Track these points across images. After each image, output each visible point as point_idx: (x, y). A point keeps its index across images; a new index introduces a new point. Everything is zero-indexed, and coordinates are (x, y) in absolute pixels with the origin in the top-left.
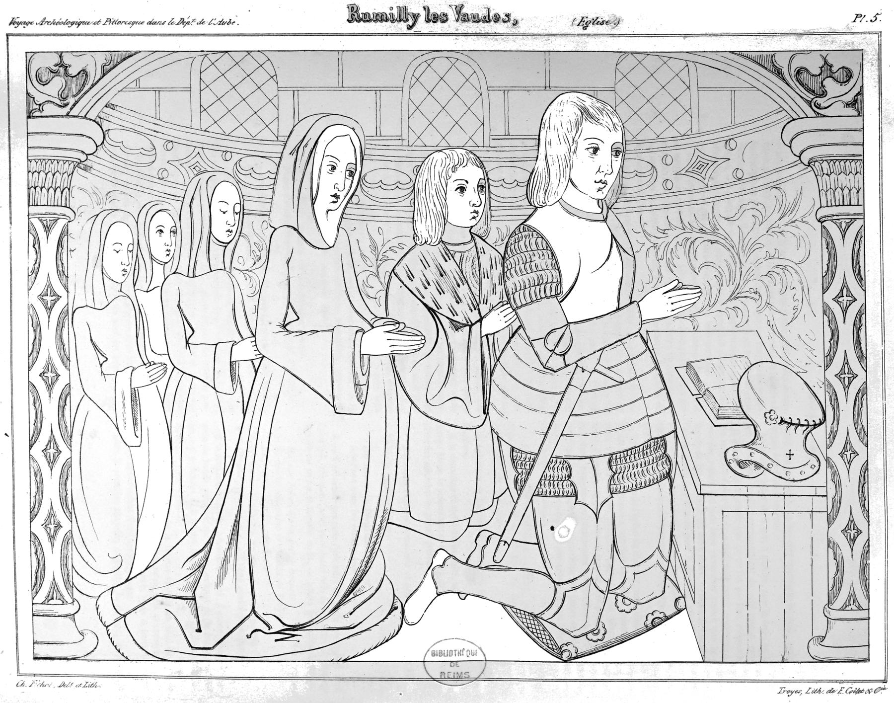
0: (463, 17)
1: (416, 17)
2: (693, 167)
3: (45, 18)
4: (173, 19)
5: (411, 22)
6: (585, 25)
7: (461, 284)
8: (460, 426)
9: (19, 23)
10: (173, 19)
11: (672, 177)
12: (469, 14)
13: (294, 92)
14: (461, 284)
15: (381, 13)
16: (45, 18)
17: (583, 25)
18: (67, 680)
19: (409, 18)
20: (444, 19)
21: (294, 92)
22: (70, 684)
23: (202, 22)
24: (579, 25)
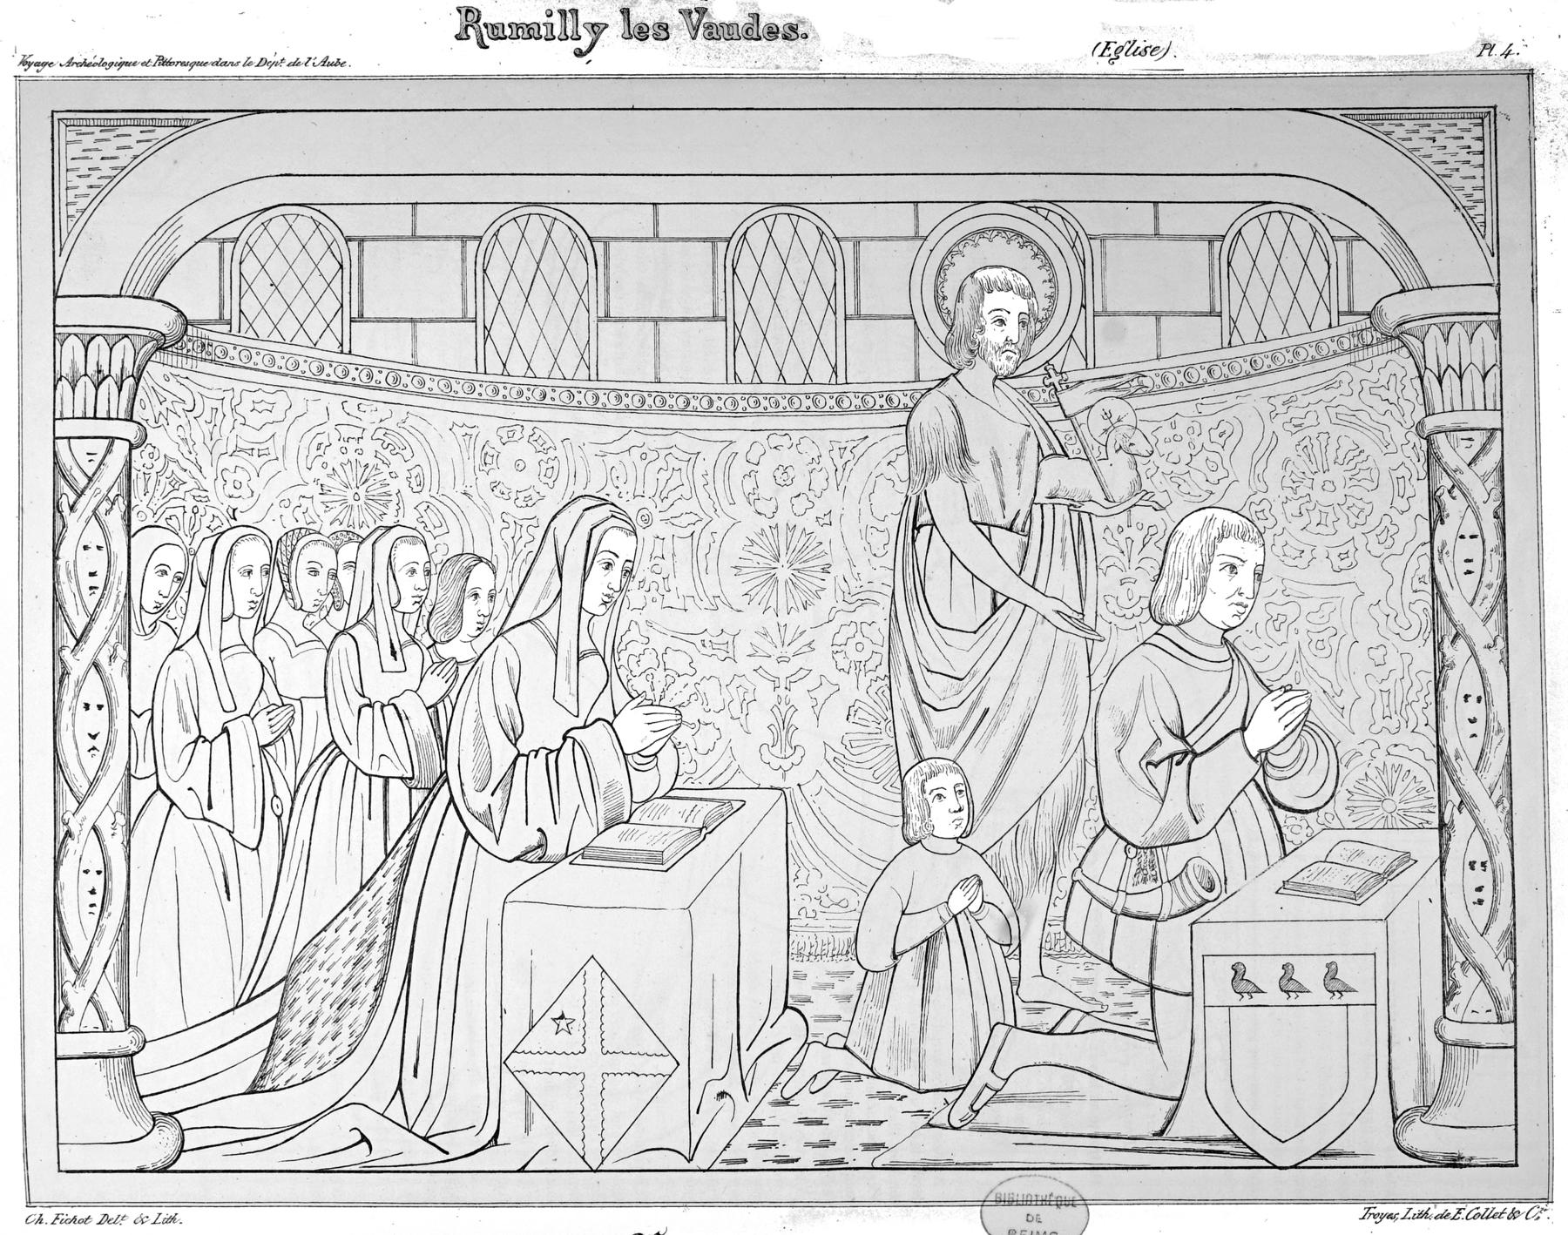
0: (701, 24)
1: (597, 29)
2: (829, 789)
3: (73, 58)
4: (249, 58)
5: (584, 44)
6: (1113, 56)
7: (1358, 786)
8: (1147, 1092)
9: (30, 64)
10: (249, 58)
11: (1383, 749)
12: (741, 25)
13: (1495, 314)
14: (1358, 786)
15: (527, 26)
16: (73, 58)
17: (1110, 55)
18: (113, 1213)
19: (582, 31)
20: (663, 31)
21: (1495, 314)
22: (120, 1218)
23: (296, 64)
24: (1102, 55)
